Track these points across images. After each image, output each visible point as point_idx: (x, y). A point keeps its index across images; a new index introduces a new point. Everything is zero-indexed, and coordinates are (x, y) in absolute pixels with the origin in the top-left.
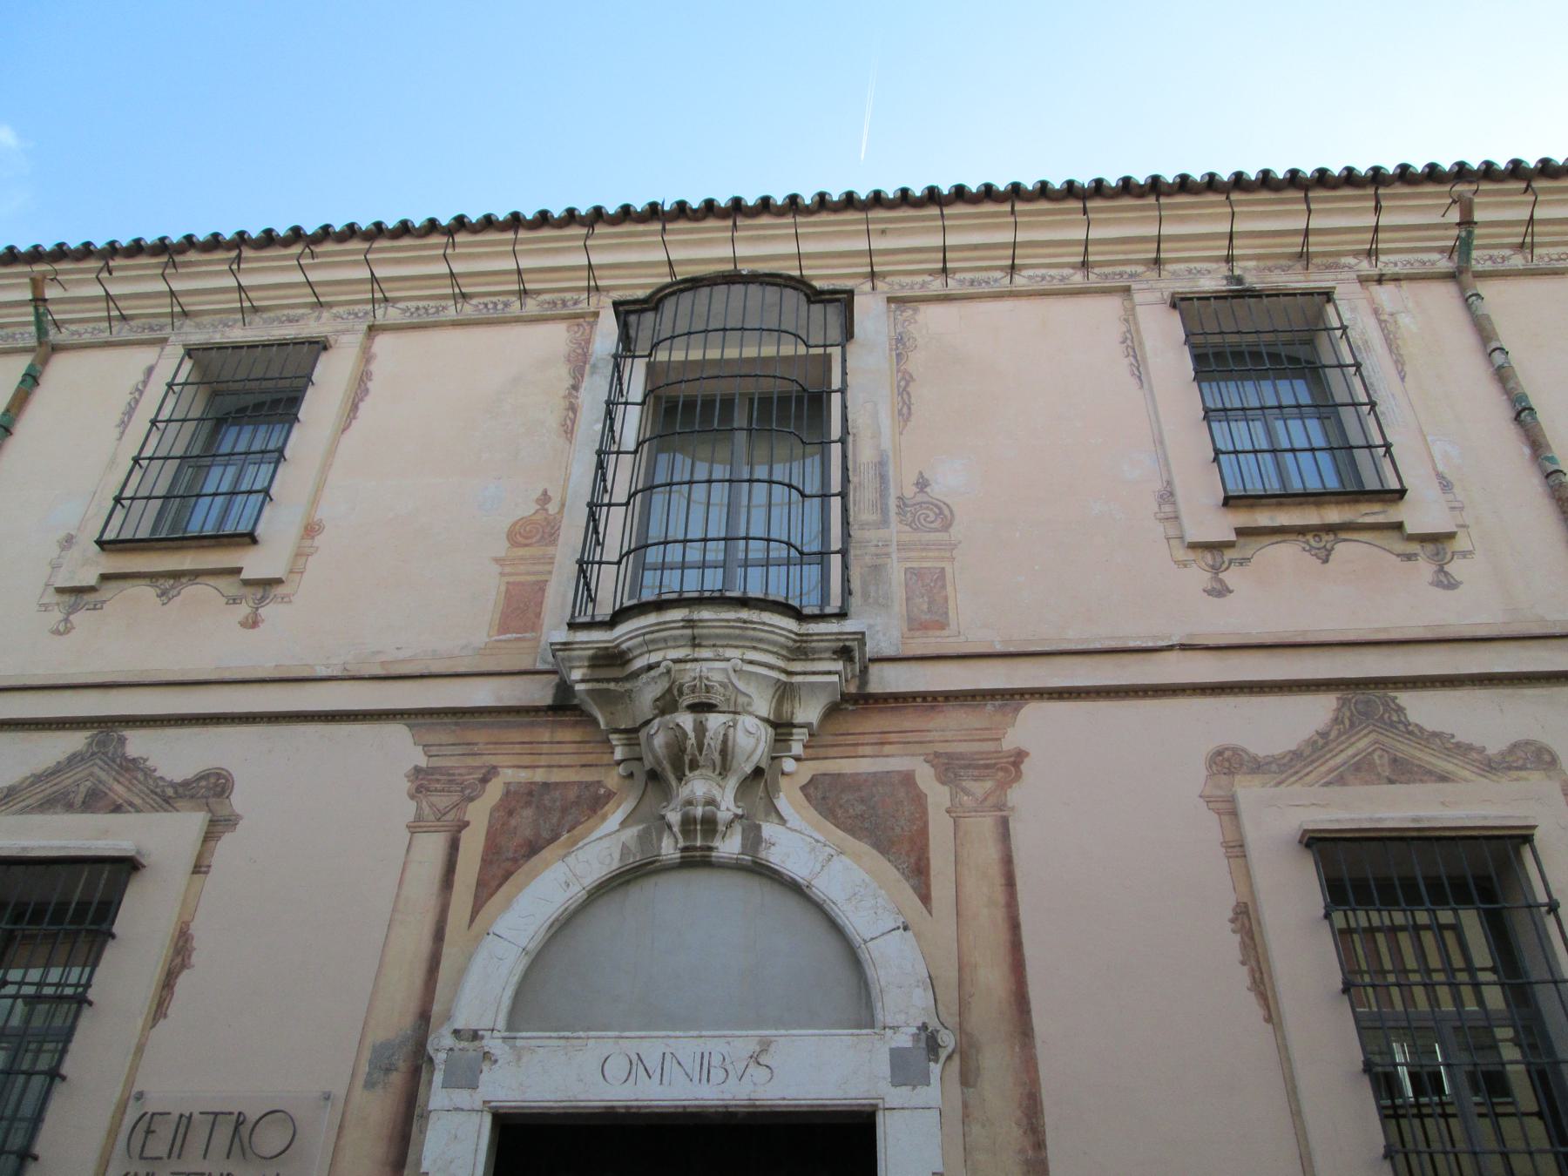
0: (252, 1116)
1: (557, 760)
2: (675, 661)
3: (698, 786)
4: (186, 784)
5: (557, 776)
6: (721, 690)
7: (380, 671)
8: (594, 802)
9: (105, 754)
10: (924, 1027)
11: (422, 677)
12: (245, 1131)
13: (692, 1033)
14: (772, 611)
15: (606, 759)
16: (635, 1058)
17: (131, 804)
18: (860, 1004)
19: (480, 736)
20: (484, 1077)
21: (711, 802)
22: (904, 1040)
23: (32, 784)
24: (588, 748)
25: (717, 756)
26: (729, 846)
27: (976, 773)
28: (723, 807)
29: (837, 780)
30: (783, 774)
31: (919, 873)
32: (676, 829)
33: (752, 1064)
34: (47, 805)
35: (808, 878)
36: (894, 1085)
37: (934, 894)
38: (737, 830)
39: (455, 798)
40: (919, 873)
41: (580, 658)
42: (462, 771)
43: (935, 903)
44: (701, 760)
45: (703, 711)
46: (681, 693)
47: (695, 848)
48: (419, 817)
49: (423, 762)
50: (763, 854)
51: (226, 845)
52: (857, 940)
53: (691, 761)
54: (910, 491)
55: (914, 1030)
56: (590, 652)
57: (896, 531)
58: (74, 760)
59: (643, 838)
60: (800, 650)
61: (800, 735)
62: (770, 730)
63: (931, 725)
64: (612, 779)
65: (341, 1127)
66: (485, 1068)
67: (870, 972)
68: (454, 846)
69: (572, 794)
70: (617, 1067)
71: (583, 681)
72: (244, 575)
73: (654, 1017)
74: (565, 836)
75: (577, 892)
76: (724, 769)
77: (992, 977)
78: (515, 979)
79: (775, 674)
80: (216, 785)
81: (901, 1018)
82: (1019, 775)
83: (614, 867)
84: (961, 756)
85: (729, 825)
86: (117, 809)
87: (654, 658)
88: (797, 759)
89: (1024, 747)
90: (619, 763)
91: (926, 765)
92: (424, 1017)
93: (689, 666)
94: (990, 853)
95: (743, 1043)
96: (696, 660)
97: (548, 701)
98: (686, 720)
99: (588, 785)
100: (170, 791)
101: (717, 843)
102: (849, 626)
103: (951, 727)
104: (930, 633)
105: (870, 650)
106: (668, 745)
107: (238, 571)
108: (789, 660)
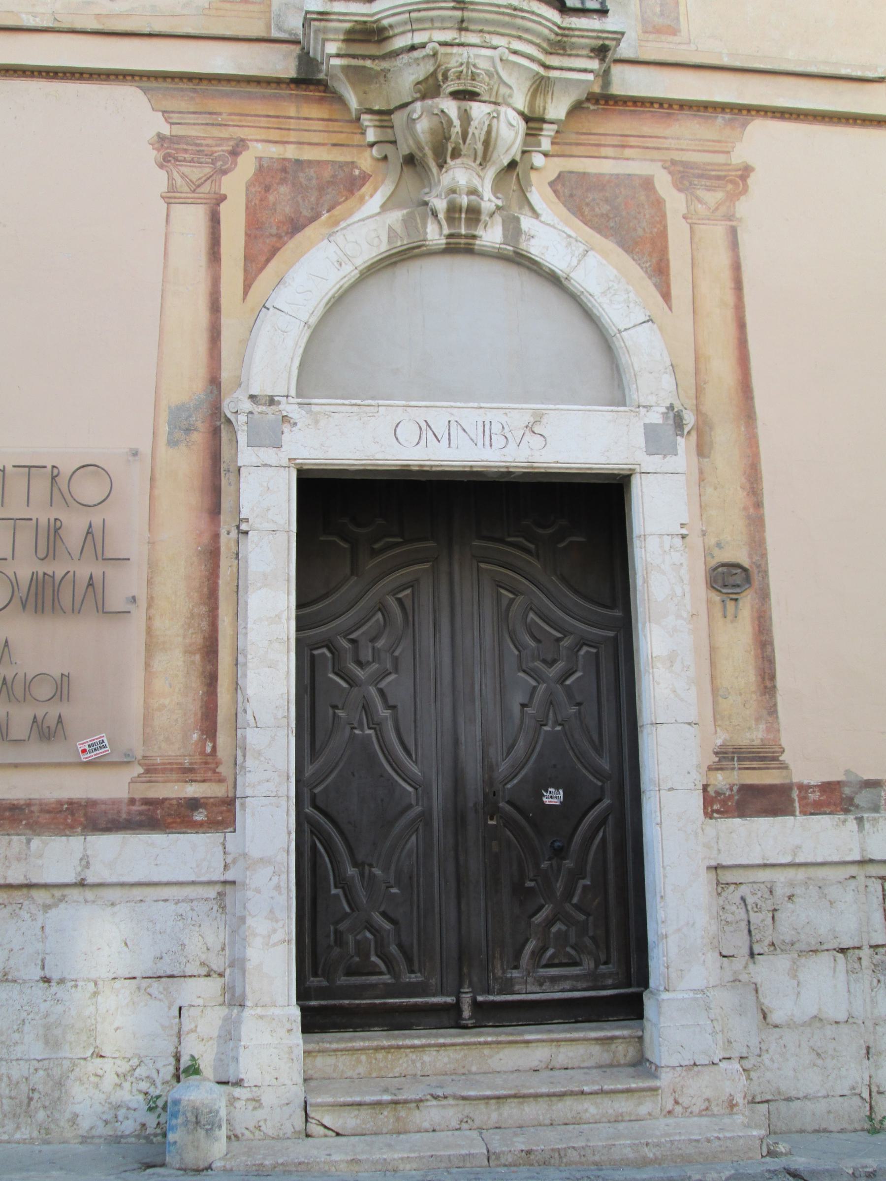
0: (66, 469)
1: (300, 137)
3: (459, 175)
5: (309, 154)
6: (487, 79)
7: (95, 25)
8: (352, 184)
10: (671, 407)
11: (150, 35)
12: (62, 482)
13: (471, 405)
15: (357, 138)
16: (423, 425)
18: (614, 381)
19: (223, 106)
20: (286, 438)
21: (473, 192)
24: (335, 126)
25: (480, 147)
26: (491, 235)
28: (486, 198)
29: (598, 183)
31: (660, 272)
32: (441, 216)
33: (528, 433)
35: (567, 270)
36: (650, 454)
37: (674, 292)
38: (498, 219)
39: (207, 170)
40: (660, 272)
41: (336, 31)
42: (210, 142)
43: (674, 301)
44: (464, 149)
45: (464, 99)
46: (445, 78)
47: (459, 236)
48: (172, 188)
49: (166, 130)
50: (523, 245)
52: (613, 330)
53: (454, 149)
56: (348, 25)
59: (407, 221)
60: (560, 44)
61: (549, 130)
63: (668, 132)
64: (366, 161)
65: (152, 479)
67: (624, 359)
68: (215, 220)
69: (327, 174)
70: (408, 432)
74: (325, 216)
75: (349, 272)
76: (485, 160)
77: (722, 368)
78: (300, 351)
79: (535, 67)
81: (652, 400)
82: (745, 190)
83: (383, 250)
85: (492, 215)
87: (419, 38)
88: (546, 155)
89: (751, 163)
90: (372, 145)
92: (215, 381)
93: (455, 50)
94: (722, 260)
95: (519, 417)
96: (462, 45)
97: (292, 73)
98: (451, 107)
99: (342, 165)
101: (479, 232)
102: (610, 23)
104: (663, 38)
105: (625, 50)
106: (432, 132)
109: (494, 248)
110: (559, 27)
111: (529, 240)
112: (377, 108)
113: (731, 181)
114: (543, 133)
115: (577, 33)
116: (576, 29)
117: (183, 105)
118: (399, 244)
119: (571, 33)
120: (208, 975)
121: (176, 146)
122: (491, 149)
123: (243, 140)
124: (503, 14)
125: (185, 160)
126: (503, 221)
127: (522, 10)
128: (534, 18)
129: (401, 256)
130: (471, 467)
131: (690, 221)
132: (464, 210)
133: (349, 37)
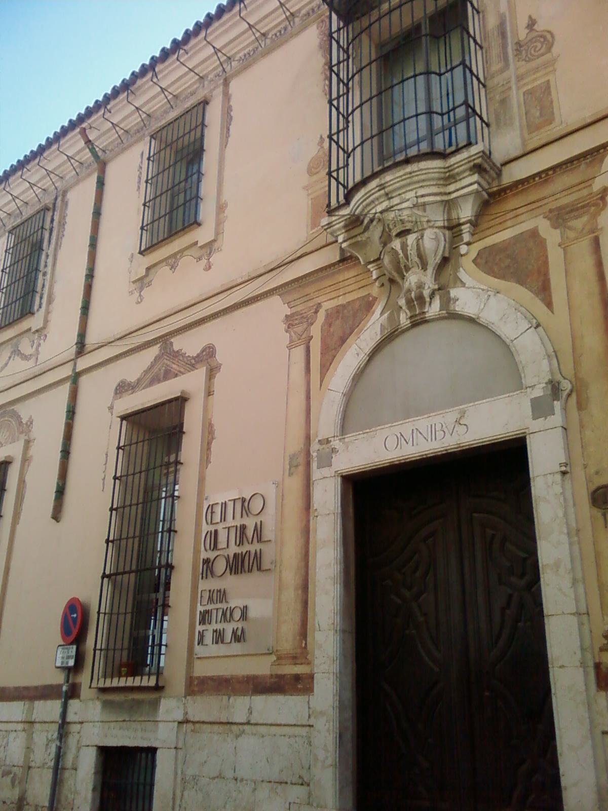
1: (347, 289)
2: (381, 212)
4: (198, 355)
8: (368, 305)
9: (167, 353)
10: (550, 382)
13: (426, 416)
14: (425, 160)
16: (399, 435)
17: (180, 372)
18: (515, 380)
22: (538, 392)
23: (145, 375)
25: (416, 259)
27: (576, 213)
30: (462, 256)
34: (151, 383)
39: (305, 325)
41: (339, 229)
47: (416, 315)
48: (291, 341)
49: (288, 312)
51: (218, 379)
52: (508, 341)
53: (405, 266)
54: (523, 34)
55: (544, 385)
56: (342, 224)
57: (516, 67)
58: (157, 359)
59: (391, 319)
61: (466, 228)
62: (447, 232)
64: (375, 290)
66: (333, 456)
70: (392, 442)
71: (344, 241)
72: (199, 245)
73: (409, 412)
75: (363, 357)
79: (438, 198)
80: (209, 352)
84: (567, 205)
86: (176, 376)
88: (468, 244)
91: (545, 220)
92: (308, 438)
95: (450, 416)
97: (338, 258)
98: (396, 244)
100: (193, 361)
103: (559, 192)
107: (196, 243)
108: (446, 185)
109: (436, 315)
110: (444, 168)
111: (455, 302)
112: (372, 260)
113: (594, 205)
114: (464, 232)
115: (456, 166)
116: (454, 164)
117: (296, 296)
118: (386, 332)
119: (452, 168)
120: (302, 784)
121: (292, 319)
122: (424, 258)
123: (319, 304)
124: (405, 179)
125: (296, 324)
126: (440, 297)
127: (414, 172)
128: (424, 172)
129: (390, 337)
130: (426, 455)
131: (563, 246)
132: (414, 299)
133: (348, 228)
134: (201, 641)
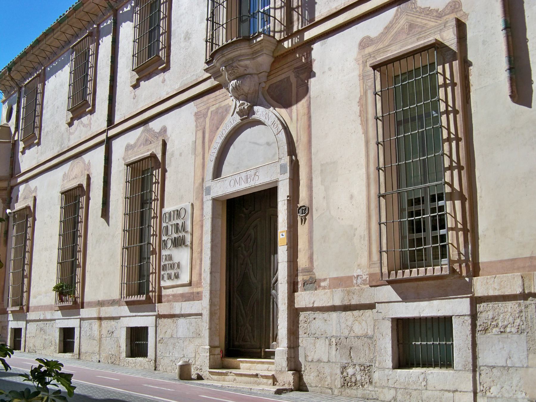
4: (160, 132)
134: (163, 279)
